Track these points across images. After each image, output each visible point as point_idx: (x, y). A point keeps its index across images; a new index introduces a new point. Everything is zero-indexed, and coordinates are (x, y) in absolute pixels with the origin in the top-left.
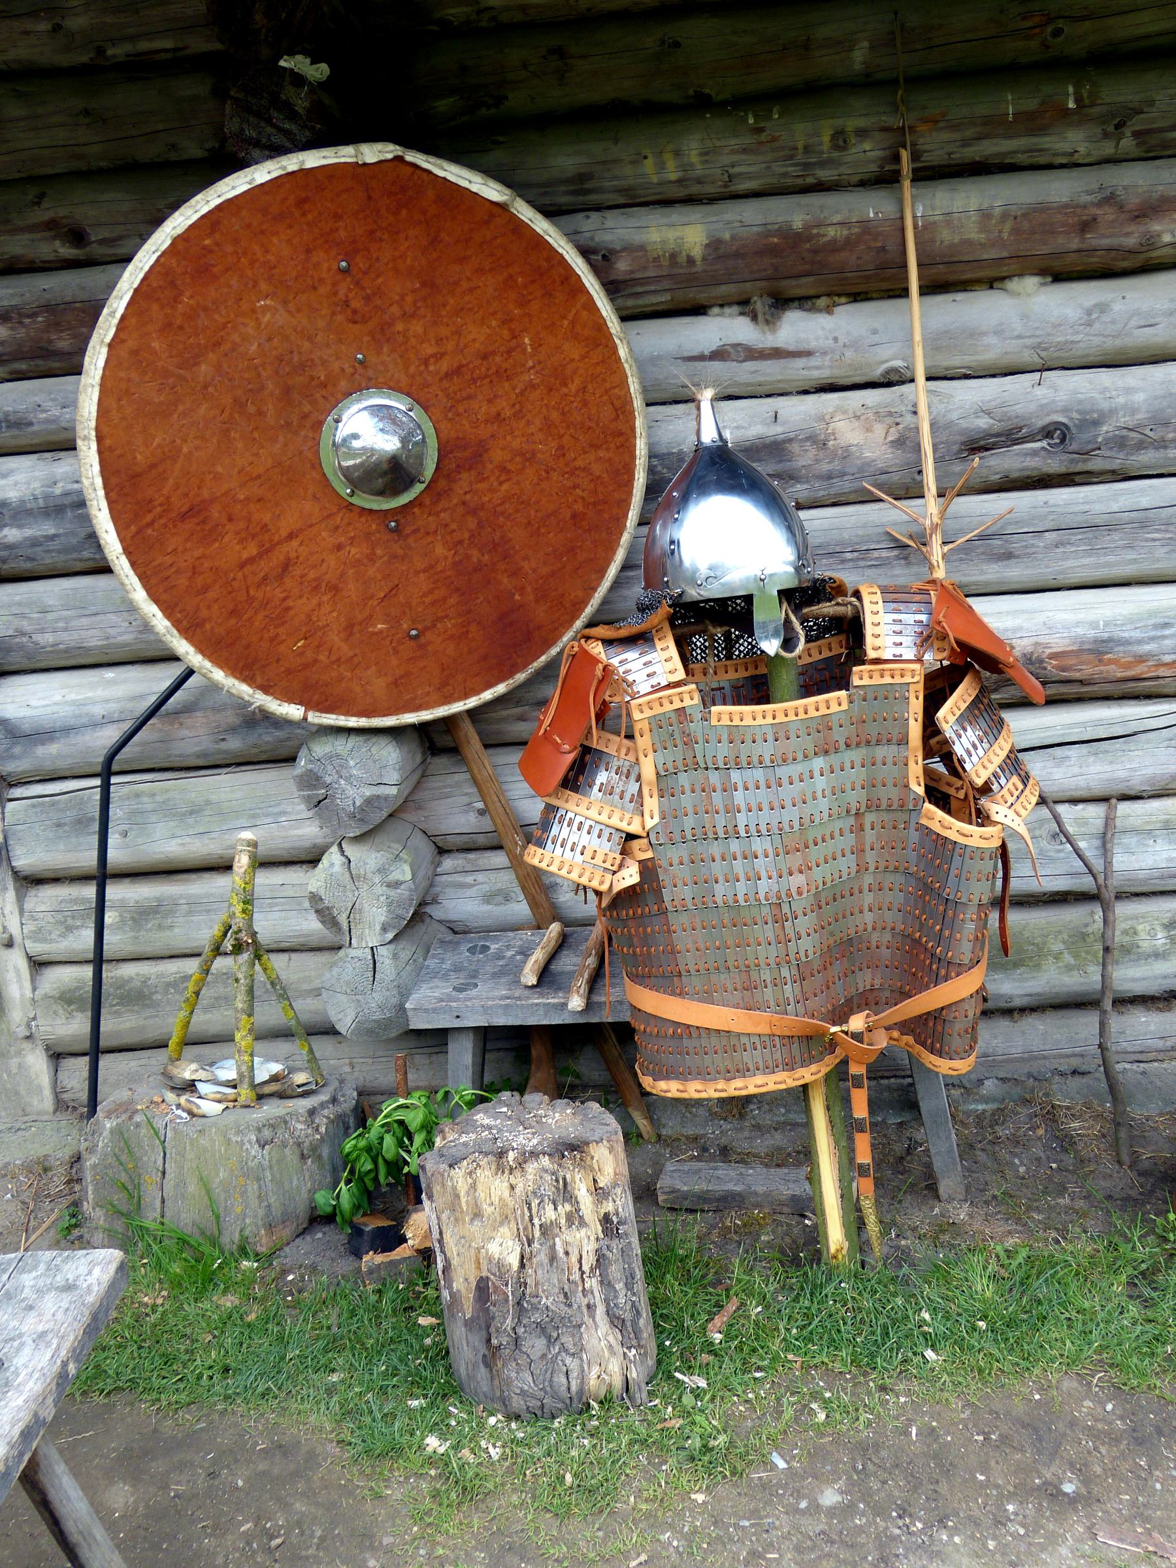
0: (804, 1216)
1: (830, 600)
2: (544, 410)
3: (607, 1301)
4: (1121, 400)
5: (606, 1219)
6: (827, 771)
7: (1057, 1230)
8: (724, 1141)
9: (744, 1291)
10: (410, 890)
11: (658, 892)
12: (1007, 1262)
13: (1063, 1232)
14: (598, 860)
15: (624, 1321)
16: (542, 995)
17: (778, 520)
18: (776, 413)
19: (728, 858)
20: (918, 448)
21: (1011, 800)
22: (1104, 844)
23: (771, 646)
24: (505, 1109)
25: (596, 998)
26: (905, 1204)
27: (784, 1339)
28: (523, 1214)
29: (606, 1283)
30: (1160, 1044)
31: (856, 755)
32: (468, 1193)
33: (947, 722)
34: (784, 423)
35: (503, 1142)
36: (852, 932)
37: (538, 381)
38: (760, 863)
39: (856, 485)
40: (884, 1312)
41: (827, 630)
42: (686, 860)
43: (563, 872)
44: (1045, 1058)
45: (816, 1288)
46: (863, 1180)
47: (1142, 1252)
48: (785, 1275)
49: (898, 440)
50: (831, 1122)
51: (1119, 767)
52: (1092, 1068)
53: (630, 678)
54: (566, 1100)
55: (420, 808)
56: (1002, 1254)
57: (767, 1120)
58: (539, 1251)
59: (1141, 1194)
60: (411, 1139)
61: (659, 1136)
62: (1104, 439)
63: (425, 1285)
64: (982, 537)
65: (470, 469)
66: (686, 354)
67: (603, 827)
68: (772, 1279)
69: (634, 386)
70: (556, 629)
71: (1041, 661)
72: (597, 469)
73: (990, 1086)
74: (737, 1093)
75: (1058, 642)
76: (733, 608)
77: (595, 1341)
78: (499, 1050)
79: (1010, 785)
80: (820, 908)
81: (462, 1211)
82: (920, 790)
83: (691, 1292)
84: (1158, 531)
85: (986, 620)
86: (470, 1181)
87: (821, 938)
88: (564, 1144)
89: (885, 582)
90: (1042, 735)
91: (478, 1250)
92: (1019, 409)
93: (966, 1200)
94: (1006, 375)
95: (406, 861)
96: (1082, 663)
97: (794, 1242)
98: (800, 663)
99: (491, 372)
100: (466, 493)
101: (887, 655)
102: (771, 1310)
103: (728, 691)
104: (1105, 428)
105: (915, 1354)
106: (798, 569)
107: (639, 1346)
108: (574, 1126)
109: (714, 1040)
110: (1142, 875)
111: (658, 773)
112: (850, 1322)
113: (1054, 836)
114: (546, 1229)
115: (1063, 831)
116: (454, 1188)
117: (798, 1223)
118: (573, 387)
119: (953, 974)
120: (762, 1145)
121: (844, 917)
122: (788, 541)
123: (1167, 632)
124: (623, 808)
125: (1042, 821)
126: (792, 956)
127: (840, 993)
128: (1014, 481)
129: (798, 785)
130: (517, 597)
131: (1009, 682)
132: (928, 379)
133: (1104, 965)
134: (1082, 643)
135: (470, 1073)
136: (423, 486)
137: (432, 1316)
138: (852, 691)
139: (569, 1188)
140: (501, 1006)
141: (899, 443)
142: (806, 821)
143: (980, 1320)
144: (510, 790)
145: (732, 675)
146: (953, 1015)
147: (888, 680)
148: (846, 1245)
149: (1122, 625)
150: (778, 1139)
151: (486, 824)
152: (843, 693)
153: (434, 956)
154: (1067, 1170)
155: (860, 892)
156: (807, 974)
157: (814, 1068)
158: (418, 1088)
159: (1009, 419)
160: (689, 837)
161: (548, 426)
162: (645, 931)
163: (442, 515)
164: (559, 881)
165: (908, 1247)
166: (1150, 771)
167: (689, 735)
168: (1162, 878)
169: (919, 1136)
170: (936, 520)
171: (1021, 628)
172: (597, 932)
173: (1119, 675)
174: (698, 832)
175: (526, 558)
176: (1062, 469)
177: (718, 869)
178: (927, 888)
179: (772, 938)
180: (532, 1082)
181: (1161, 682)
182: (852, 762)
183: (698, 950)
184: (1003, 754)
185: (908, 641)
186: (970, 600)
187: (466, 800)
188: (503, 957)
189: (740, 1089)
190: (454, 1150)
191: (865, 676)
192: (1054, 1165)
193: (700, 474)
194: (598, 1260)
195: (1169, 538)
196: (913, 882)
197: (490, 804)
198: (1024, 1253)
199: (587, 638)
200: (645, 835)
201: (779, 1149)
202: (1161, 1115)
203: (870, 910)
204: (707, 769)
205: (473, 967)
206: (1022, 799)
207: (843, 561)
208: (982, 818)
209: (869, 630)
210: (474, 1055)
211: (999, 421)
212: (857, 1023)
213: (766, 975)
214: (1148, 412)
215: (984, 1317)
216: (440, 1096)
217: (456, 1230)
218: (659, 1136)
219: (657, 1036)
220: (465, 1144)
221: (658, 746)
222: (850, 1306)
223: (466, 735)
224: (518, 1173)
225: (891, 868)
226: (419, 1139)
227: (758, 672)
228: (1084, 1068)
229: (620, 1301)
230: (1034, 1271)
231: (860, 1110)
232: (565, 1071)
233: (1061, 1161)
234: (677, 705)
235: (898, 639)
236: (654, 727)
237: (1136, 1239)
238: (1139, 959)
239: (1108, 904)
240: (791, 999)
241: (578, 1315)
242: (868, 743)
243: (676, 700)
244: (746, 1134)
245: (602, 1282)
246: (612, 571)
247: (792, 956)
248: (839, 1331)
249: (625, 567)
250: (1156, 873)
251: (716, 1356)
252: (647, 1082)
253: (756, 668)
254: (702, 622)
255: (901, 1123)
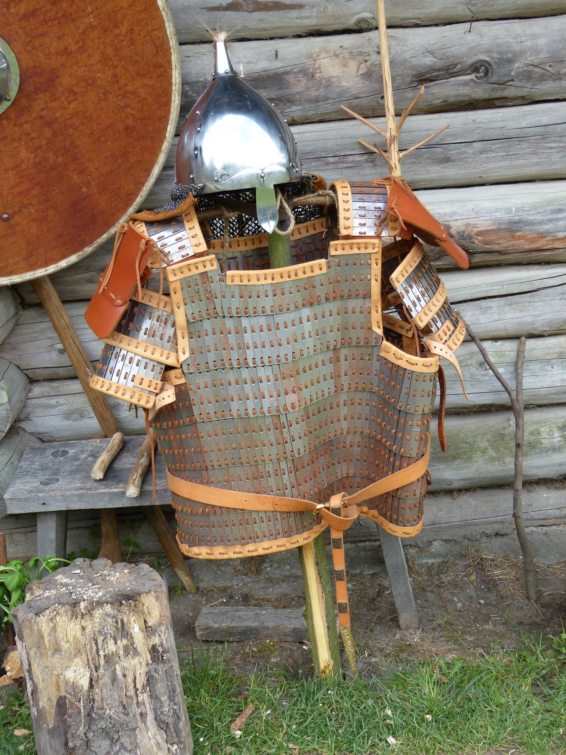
0: (302, 643)
1: (313, 192)
2: (101, 46)
3: (155, 710)
4: (529, 44)
5: (153, 650)
6: (312, 318)
7: (483, 647)
8: (245, 591)
9: (258, 699)
10: (7, 410)
11: (189, 409)
12: (447, 671)
13: (487, 650)
14: (145, 385)
15: (167, 724)
16: (107, 486)
17: (273, 132)
18: (277, 52)
19: (240, 382)
20: (380, 79)
21: (445, 338)
22: (516, 370)
23: (269, 226)
24: (78, 571)
25: (147, 488)
26: (375, 632)
27: (287, 733)
28: (91, 648)
29: (154, 697)
30: (557, 513)
31: (333, 306)
32: (50, 635)
33: (398, 282)
34: (283, 60)
35: (76, 595)
36: (332, 435)
37: (96, 23)
38: (264, 386)
39: (336, 107)
40: (359, 710)
41: (312, 214)
42: (209, 385)
43: (119, 395)
44: (476, 524)
45: (310, 695)
46: (342, 615)
47: (543, 661)
48: (288, 686)
49: (367, 73)
50: (320, 575)
51: (526, 314)
52: (509, 531)
53: (166, 250)
54: (124, 563)
55: (15, 349)
56: (444, 666)
57: (277, 574)
58: (104, 675)
59: (543, 620)
60: (10, 597)
61: (198, 588)
62: (516, 73)
63: (21, 705)
64: (428, 146)
65: (46, 90)
66: (209, 5)
67: (148, 361)
68: (278, 689)
69: (170, 29)
70: (114, 214)
71: (471, 237)
72: (143, 93)
73: (437, 546)
74: (250, 554)
75: (483, 224)
76: (244, 199)
77: (146, 740)
78: (78, 528)
79: (444, 327)
80: (308, 418)
81: (45, 648)
82: (380, 332)
83: (219, 701)
84: (554, 141)
85: (428, 208)
86: (51, 625)
87: (309, 439)
88: (122, 595)
89: (356, 179)
90: (472, 291)
91: (58, 676)
92: (455, 51)
93: (419, 628)
94: (446, 24)
95: (3, 389)
96: (500, 239)
97: (295, 662)
98: (292, 238)
99: (59, 15)
100: (43, 109)
101: (356, 233)
102: (277, 713)
103: (240, 259)
104: (517, 65)
105: (380, 740)
106: (289, 169)
107: (180, 742)
108: (130, 581)
109: (232, 516)
110: (543, 391)
111: (188, 321)
112: (334, 719)
113: (481, 364)
114: (109, 658)
115: (487, 361)
116: (39, 631)
117: (299, 648)
118: (124, 29)
119: (405, 465)
120: (273, 592)
121: (326, 425)
122: (281, 149)
123: (560, 216)
124: (162, 347)
125: (472, 354)
126: (289, 454)
127: (324, 479)
128: (452, 104)
129: (291, 329)
130: (84, 190)
131: (443, 254)
132: (389, 27)
133: (516, 457)
134: (500, 224)
135: (54, 545)
136: (9, 104)
137: (25, 728)
138: (330, 259)
139: (126, 627)
140: (76, 495)
141: (367, 75)
142: (297, 355)
143: (427, 714)
144: (83, 335)
145: (243, 248)
146: (405, 494)
147: (355, 251)
148: (332, 663)
149: (528, 211)
150: (284, 588)
151: (65, 360)
152: (323, 261)
153: (26, 460)
154: (491, 605)
155: (338, 406)
156: (300, 466)
157: (305, 535)
158: (13, 559)
159: (448, 57)
160: (212, 367)
161: (105, 59)
162: (181, 438)
163: (25, 126)
164: (120, 402)
165: (377, 663)
166: (548, 317)
167: (210, 292)
168: (557, 393)
169: (386, 584)
170: (394, 133)
171: (455, 213)
172: (147, 441)
173: (526, 247)
174: (219, 363)
175: (90, 160)
176: (486, 96)
177: (233, 390)
178: (385, 403)
179: (273, 440)
180: (102, 551)
181: (556, 252)
182: (331, 311)
183: (219, 450)
184: (439, 305)
185: (370, 222)
186: (415, 193)
187: (49, 342)
188: (79, 459)
189: (252, 551)
190: (40, 602)
191: (339, 248)
192: (482, 602)
193: (216, 97)
194: (148, 680)
195: (562, 147)
196: (376, 399)
197: (67, 345)
198: (459, 665)
199: (134, 220)
200: (179, 366)
201: (286, 595)
202: (558, 563)
203: (345, 419)
204: (224, 317)
205: (56, 467)
206: (453, 337)
207: (327, 164)
208: (424, 351)
209: (342, 215)
210: (57, 533)
211: (441, 59)
212: (336, 501)
213: (270, 468)
214: (548, 53)
215: (430, 712)
216: (31, 563)
217: (41, 662)
218: (198, 588)
219: (191, 514)
220: (48, 598)
221: (188, 300)
222: (334, 706)
223: (48, 294)
224: (87, 618)
225: (360, 388)
226: (15, 596)
227: (262, 245)
228: (504, 531)
229: (165, 709)
230: (466, 677)
231: (340, 565)
232: (127, 543)
233: (487, 598)
234: (201, 270)
235: (363, 221)
236: (185, 286)
237: (539, 652)
238: (542, 452)
239: (519, 413)
240: (288, 485)
241: (134, 721)
242: (342, 297)
243: (200, 266)
244: (262, 585)
245: (151, 696)
246: (156, 170)
247: (289, 454)
248: (326, 725)
249: (166, 167)
250: (553, 391)
251: (237, 747)
252: (184, 548)
253: (261, 242)
254: (219, 208)
255: (374, 574)
